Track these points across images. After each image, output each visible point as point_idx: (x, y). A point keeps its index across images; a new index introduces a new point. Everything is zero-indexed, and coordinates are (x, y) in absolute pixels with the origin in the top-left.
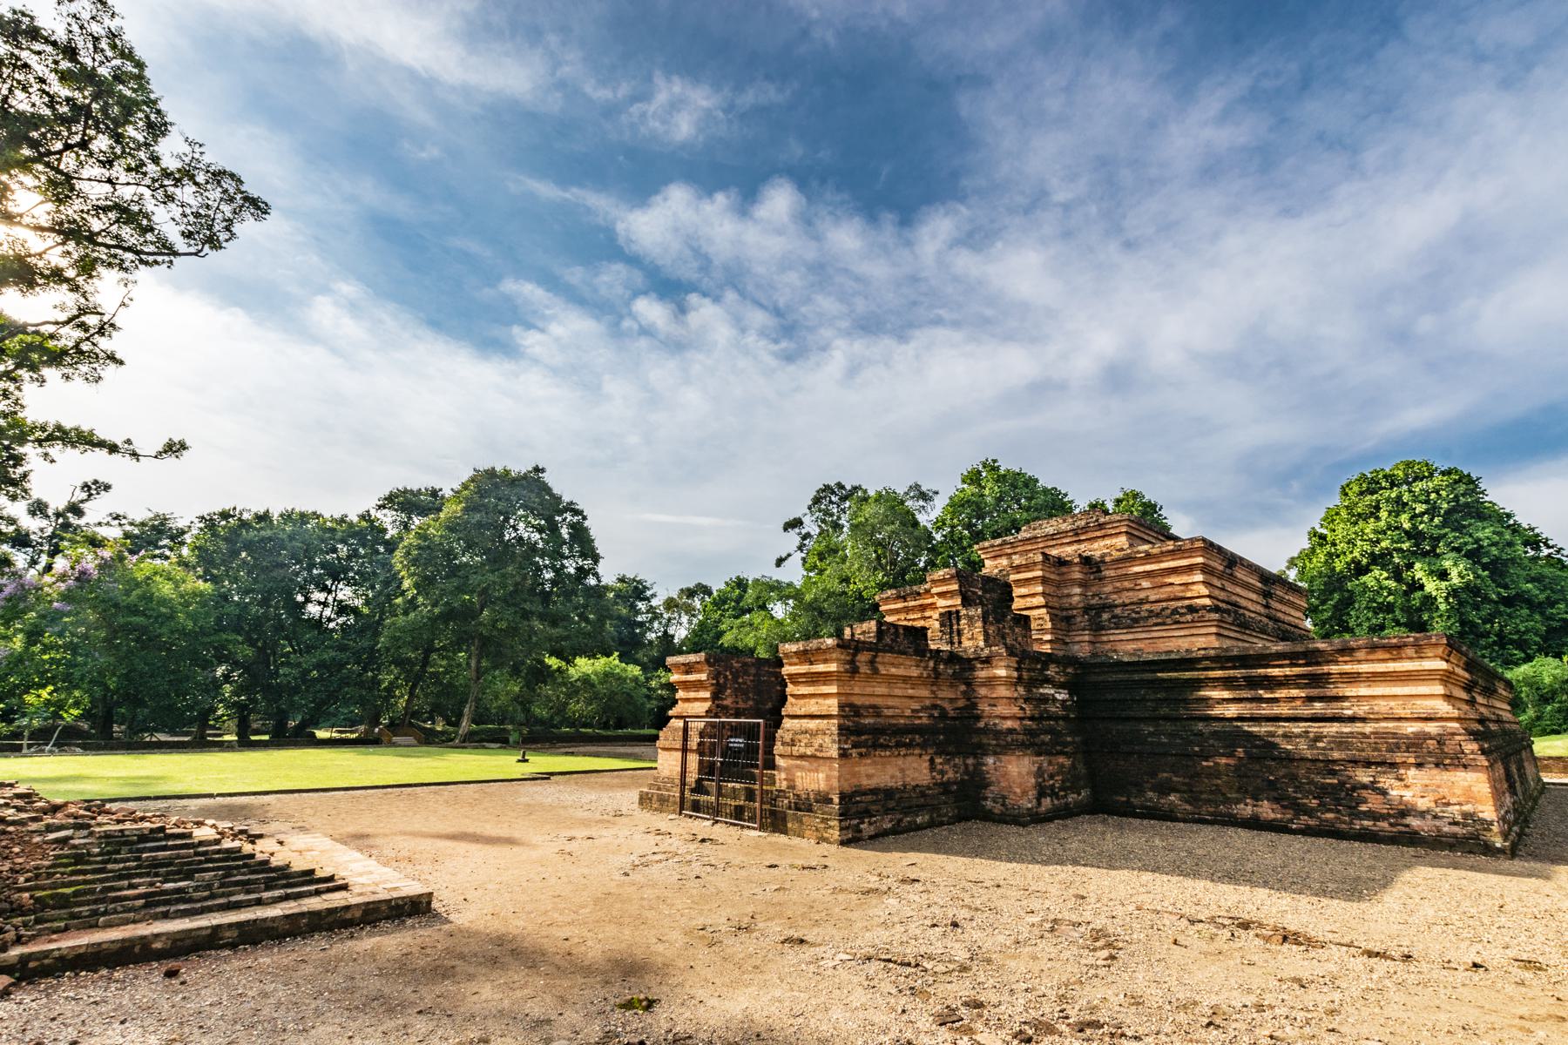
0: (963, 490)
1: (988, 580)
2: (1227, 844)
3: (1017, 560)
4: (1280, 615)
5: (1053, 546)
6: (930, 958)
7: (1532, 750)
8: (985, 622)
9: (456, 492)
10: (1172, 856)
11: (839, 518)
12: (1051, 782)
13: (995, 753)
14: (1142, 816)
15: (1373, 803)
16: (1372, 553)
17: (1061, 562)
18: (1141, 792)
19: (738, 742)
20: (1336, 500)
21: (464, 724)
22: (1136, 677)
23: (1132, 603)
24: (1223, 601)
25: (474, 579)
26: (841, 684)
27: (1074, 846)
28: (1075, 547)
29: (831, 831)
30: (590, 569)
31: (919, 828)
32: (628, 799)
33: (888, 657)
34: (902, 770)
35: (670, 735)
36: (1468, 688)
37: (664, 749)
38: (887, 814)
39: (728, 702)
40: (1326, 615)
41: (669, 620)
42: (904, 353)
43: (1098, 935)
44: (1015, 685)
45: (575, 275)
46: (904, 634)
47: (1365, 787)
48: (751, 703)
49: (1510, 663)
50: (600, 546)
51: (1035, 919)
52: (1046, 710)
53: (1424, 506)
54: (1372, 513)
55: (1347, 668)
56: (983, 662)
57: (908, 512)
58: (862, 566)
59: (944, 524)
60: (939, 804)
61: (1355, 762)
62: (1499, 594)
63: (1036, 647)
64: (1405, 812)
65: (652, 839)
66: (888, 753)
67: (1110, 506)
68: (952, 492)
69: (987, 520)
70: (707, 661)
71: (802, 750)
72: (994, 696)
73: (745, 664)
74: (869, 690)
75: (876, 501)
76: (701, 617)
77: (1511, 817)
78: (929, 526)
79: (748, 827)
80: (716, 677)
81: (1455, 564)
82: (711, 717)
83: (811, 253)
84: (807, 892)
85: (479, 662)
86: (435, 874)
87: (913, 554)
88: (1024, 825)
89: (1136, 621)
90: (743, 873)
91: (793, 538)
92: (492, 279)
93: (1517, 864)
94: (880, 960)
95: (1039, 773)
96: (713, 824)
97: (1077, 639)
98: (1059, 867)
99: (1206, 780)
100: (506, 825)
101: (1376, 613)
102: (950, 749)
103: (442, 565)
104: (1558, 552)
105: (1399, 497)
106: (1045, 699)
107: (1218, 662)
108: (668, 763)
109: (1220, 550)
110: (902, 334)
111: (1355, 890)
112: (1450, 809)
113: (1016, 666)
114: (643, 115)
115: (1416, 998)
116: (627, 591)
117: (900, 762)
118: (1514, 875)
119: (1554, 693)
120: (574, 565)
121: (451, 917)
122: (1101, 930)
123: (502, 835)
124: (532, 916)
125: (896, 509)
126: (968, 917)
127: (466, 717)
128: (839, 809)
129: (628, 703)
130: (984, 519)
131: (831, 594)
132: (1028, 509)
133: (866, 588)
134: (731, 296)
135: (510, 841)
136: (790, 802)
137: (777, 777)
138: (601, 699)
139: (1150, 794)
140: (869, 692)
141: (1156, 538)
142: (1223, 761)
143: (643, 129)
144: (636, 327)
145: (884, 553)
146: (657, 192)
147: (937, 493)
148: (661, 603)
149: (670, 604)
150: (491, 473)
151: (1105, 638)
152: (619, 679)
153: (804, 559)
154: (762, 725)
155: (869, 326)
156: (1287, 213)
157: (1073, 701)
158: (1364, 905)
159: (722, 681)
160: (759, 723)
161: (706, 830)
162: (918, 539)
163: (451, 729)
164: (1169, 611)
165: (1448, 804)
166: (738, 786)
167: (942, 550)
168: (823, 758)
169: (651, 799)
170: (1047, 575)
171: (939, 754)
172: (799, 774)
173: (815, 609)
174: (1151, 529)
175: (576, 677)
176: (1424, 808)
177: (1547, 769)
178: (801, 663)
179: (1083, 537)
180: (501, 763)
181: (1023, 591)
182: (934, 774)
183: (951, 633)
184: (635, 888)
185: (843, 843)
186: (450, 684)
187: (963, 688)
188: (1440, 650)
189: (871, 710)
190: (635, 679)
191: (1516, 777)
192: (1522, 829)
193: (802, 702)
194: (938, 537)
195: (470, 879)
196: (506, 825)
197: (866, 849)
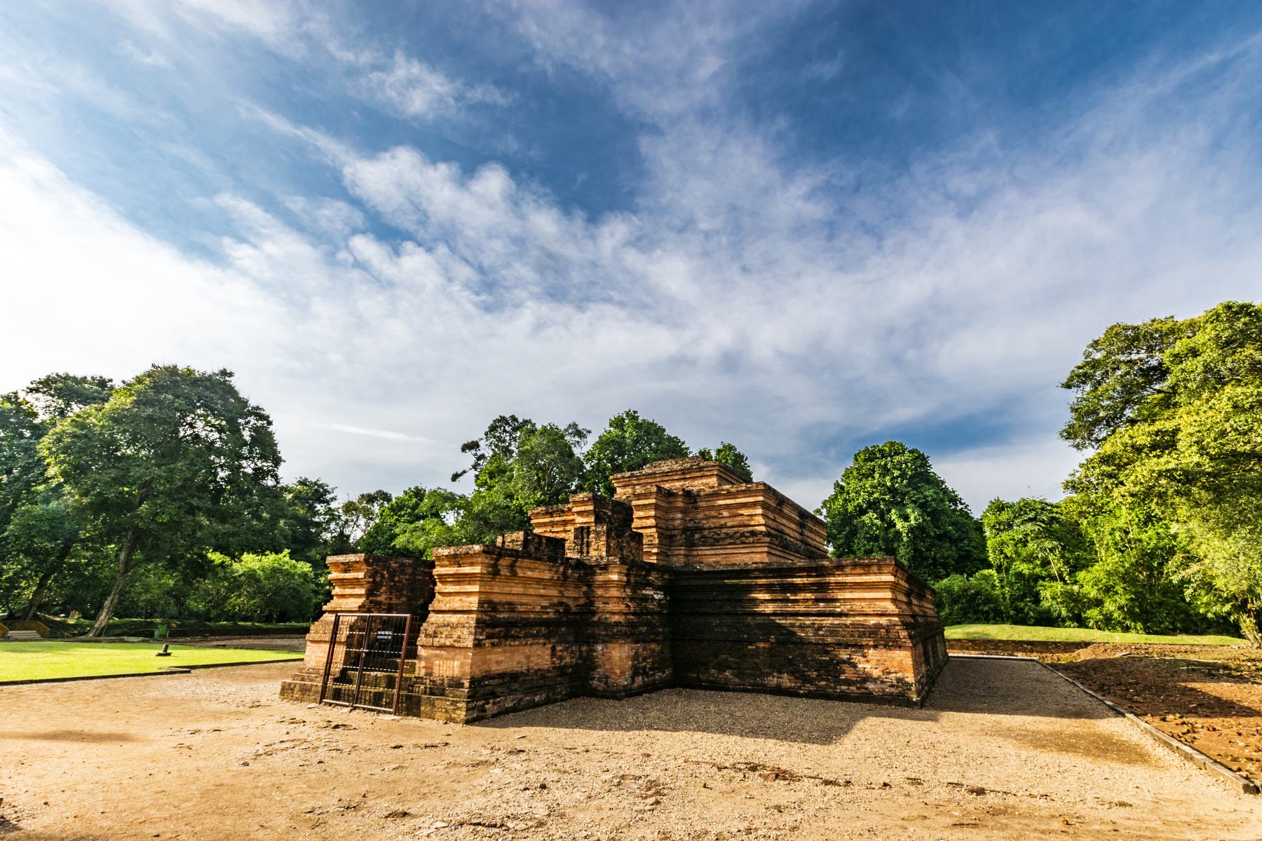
0: (610, 432)
1: (619, 504)
2: (758, 707)
3: (639, 490)
4: (809, 540)
5: (667, 481)
6: (515, 818)
7: (943, 636)
8: (608, 537)
9: (128, 385)
10: (719, 718)
11: (510, 445)
12: (644, 664)
13: (604, 642)
14: (705, 688)
15: (848, 674)
16: (869, 502)
17: (670, 494)
18: (707, 669)
19: (387, 634)
20: (851, 464)
21: (102, 617)
22: (711, 582)
23: (716, 528)
24: (773, 529)
25: (135, 472)
26: (483, 583)
27: (653, 714)
28: (681, 483)
29: (458, 712)
30: (269, 471)
31: (537, 705)
32: (269, 690)
33: (526, 562)
34: (528, 657)
35: (320, 629)
36: (908, 594)
37: (313, 642)
38: (510, 695)
39: (382, 598)
40: (841, 541)
41: (347, 522)
42: (580, 321)
43: (652, 784)
44: (624, 587)
45: (297, 204)
46: (547, 544)
47: (844, 662)
48: (404, 599)
49: (938, 578)
50: (283, 450)
51: (608, 776)
52: (646, 608)
53: (899, 472)
54: (871, 474)
55: (840, 579)
56: (602, 569)
57: (566, 445)
58: (524, 486)
59: (593, 457)
60: (556, 684)
61: (839, 645)
62: (935, 532)
63: (646, 559)
64: (867, 678)
65: (284, 727)
66: (517, 643)
67: (713, 454)
68: (602, 432)
69: (626, 457)
70: (366, 561)
71: (442, 641)
72: (608, 595)
73: (402, 565)
74: (506, 590)
75: (541, 433)
76: (377, 521)
77: (924, 680)
78: (582, 458)
79: (385, 712)
80: (373, 575)
81: (913, 512)
82: (363, 612)
83: (515, 228)
84: (423, 768)
85: (129, 555)
86: (16, 778)
87: (567, 479)
88: (619, 699)
89: (717, 540)
90: (368, 755)
91: (470, 458)
92: (210, 191)
93: (924, 712)
94: (471, 824)
95: (636, 657)
96: (351, 711)
97: (677, 552)
98: (637, 732)
99: (750, 660)
100: (123, 721)
101: (869, 542)
102: (569, 639)
103: (100, 455)
104: (966, 507)
105: (886, 464)
106: (646, 599)
107: (763, 573)
108: (314, 655)
109: (774, 491)
110: (581, 305)
111: (828, 736)
112: (890, 676)
113: (626, 572)
114: (381, 83)
115: (847, 812)
116: (307, 494)
117: (527, 650)
118: (920, 720)
119: (959, 597)
120: (252, 466)
121: (21, 825)
122: (654, 781)
123: (115, 732)
124: (124, 814)
125: (556, 441)
126: (556, 779)
127: (105, 610)
128: (468, 692)
129: (293, 597)
130: (623, 456)
131: (496, 507)
132: (655, 451)
133: (526, 504)
134: (442, 250)
135: (122, 738)
136: (425, 688)
137: (417, 666)
138: (265, 594)
139: (713, 671)
140: (504, 591)
141: (737, 481)
142: (762, 645)
143: (379, 95)
144: (351, 259)
145: (544, 476)
146: (386, 150)
147: (590, 432)
148: (341, 506)
149: (350, 508)
150: (173, 371)
151: (695, 553)
152: (288, 574)
153: (477, 477)
154: (409, 619)
155: (556, 294)
156: (841, 269)
157: (667, 601)
158: (831, 747)
159: (378, 579)
160: (406, 618)
161: (343, 716)
162: (572, 468)
163: (87, 622)
164: (739, 535)
165: (890, 673)
166: (379, 674)
167: (590, 477)
168: (460, 648)
169: (292, 690)
170: (659, 503)
171: (559, 643)
172: (437, 662)
173: (481, 519)
174: (734, 474)
175: (241, 572)
176: (876, 676)
177: (952, 647)
178: (450, 565)
179: (688, 476)
180: (137, 657)
181: (641, 514)
182: (554, 659)
183: (582, 544)
184: (251, 777)
185: (468, 722)
186: (93, 576)
187: (585, 589)
188: (891, 569)
189: (506, 606)
190: (304, 575)
191: (931, 653)
192: (930, 689)
193: (448, 599)
194: (588, 467)
195: (60, 780)
196: (123, 721)
197: (487, 726)
